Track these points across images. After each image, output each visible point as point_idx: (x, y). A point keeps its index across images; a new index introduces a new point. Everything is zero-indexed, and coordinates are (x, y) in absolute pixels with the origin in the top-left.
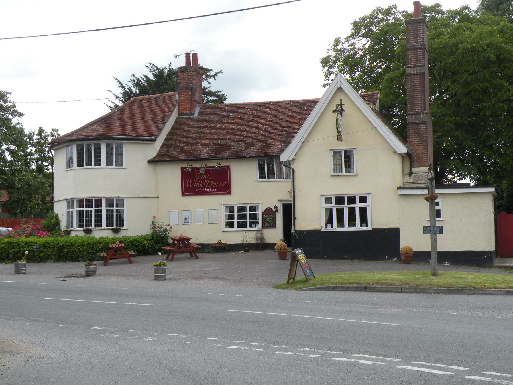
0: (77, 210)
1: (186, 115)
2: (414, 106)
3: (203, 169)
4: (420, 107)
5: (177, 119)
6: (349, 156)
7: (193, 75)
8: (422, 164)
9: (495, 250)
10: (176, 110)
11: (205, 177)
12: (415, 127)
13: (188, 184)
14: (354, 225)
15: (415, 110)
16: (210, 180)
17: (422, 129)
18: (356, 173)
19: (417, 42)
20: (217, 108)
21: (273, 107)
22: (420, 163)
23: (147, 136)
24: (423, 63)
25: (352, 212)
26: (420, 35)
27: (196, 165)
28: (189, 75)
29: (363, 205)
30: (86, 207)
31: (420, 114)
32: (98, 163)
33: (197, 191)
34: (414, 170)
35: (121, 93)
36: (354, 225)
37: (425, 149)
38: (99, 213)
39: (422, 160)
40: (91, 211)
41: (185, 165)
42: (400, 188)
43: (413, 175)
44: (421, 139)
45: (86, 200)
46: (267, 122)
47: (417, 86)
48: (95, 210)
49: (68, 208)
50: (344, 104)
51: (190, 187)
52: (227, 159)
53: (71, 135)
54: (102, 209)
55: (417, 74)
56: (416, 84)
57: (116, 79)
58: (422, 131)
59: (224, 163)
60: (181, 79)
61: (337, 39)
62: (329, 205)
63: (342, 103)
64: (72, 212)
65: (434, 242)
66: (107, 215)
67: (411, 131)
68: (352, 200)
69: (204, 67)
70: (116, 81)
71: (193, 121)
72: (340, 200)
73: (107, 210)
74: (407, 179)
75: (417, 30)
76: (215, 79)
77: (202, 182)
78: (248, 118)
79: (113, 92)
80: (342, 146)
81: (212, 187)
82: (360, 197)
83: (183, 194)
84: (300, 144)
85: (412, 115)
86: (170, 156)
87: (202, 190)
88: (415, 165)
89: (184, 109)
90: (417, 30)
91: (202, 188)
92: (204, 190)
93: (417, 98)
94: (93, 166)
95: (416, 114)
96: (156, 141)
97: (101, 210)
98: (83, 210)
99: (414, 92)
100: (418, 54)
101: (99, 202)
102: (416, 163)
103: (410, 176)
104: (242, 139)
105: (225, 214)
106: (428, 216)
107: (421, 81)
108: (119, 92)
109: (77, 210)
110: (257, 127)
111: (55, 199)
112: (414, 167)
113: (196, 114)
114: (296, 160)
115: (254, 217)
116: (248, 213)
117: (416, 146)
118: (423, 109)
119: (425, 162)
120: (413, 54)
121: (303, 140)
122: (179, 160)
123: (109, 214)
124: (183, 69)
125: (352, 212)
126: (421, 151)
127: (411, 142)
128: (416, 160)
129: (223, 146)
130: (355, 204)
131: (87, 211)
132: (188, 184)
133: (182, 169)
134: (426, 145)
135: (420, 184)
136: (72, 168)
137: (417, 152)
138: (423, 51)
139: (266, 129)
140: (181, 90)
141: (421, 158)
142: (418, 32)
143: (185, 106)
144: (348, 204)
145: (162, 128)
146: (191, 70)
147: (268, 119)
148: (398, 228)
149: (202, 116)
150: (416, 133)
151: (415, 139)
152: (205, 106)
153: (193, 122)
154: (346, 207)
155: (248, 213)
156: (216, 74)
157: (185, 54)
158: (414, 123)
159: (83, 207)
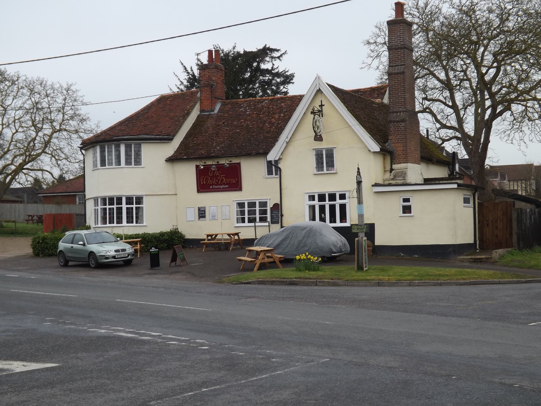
0: (101, 208)
1: (207, 112)
2: (395, 104)
3: (214, 166)
4: (401, 105)
5: (198, 116)
6: (330, 154)
7: (213, 72)
8: (402, 161)
9: (375, 245)
10: (197, 107)
11: (218, 174)
12: (395, 125)
13: (203, 181)
15: (396, 108)
16: (222, 177)
17: (402, 126)
18: (336, 171)
19: (398, 42)
20: (237, 104)
21: (289, 102)
22: (400, 160)
23: (166, 134)
24: (403, 63)
25: (332, 208)
26: (401, 35)
27: (209, 163)
28: (210, 73)
29: (342, 202)
30: (109, 205)
31: (400, 112)
32: (119, 163)
33: (211, 187)
34: (395, 166)
35: (186, 79)
36: (335, 222)
37: (405, 146)
38: (120, 210)
39: (402, 157)
40: (113, 208)
41: (201, 164)
42: (376, 185)
43: (393, 172)
44: (401, 136)
45: (109, 198)
46: (281, 118)
47: (397, 84)
48: (117, 207)
49: (95, 206)
50: (324, 105)
51: (205, 183)
53: (100, 135)
54: (126, 205)
55: (397, 73)
56: (397, 82)
57: (182, 64)
58: (401, 128)
59: (235, 161)
60: (202, 77)
62: (312, 203)
63: (323, 104)
64: (97, 209)
66: (128, 213)
68: (332, 197)
69: (270, 47)
70: (181, 66)
71: (212, 118)
72: (322, 197)
73: (127, 208)
74: (388, 175)
75: (398, 30)
76: (280, 60)
77: (216, 179)
78: (264, 113)
79: (179, 77)
81: (224, 184)
82: (248, 202)
83: (199, 191)
84: (285, 145)
85: (393, 112)
86: (185, 155)
87: (216, 187)
88: (396, 161)
89: (205, 106)
90: (398, 30)
91: (216, 185)
92: (217, 187)
93: (398, 96)
95: (397, 112)
97: (122, 207)
98: (106, 208)
99: (395, 91)
100: (398, 53)
101: (119, 200)
102: (396, 160)
103: (391, 172)
104: (254, 135)
105: (237, 210)
106: (400, 211)
107: (401, 80)
108: (184, 77)
109: (101, 208)
110: (270, 123)
111: (87, 197)
112: (395, 164)
113: (216, 111)
114: (282, 160)
115: (264, 212)
116: (257, 208)
117: (397, 143)
118: (404, 107)
119: (404, 158)
120: (395, 54)
121: (287, 140)
122: (193, 158)
123: (129, 211)
124: (204, 67)
125: (332, 208)
126: (401, 148)
127: (392, 139)
128: (396, 157)
129: (235, 143)
130: (336, 201)
131: (109, 208)
132: (203, 181)
133: (197, 167)
134: (405, 142)
135: (399, 181)
136: (96, 168)
137: (398, 149)
138: (403, 51)
139: (278, 124)
140: (203, 87)
141: (401, 155)
142: (399, 32)
143: (206, 103)
144: (329, 201)
145: (180, 126)
146: (212, 67)
147: (282, 115)
148: (374, 224)
149: (221, 113)
150: (397, 131)
151: (396, 137)
152: (225, 102)
153: (212, 119)
154: (327, 203)
155: (257, 208)
156: (281, 56)
157: (208, 52)
159: (106, 205)
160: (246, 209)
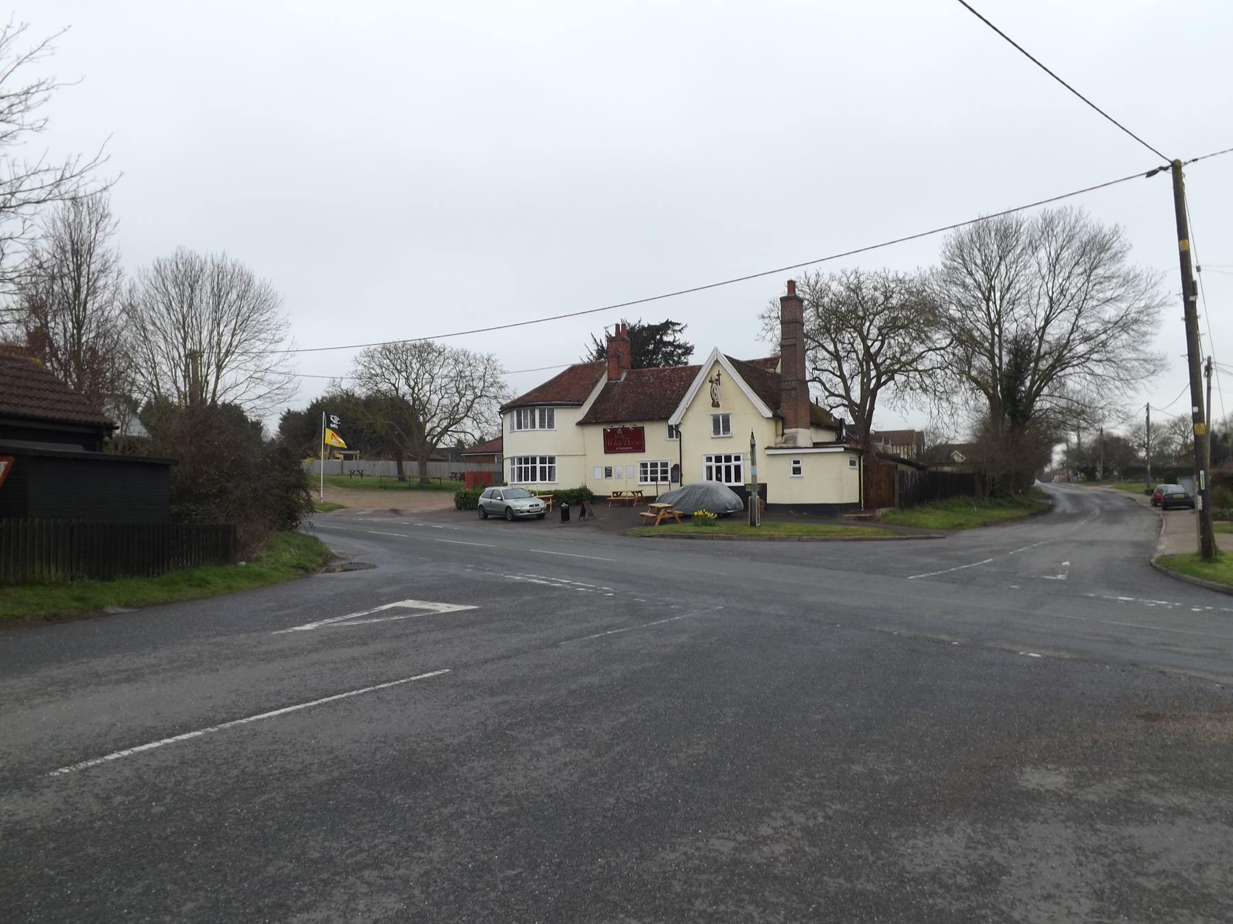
6: (726, 420)
14: (730, 481)
25: (728, 469)
34: (785, 431)
36: (730, 481)
38: (534, 469)
41: (608, 428)
42: (768, 448)
52: (640, 421)
59: (639, 425)
61: (981, 228)
62: (709, 464)
65: (1148, 486)
67: (784, 397)
68: (728, 459)
72: (718, 459)
74: (779, 439)
80: (720, 411)
81: (629, 446)
83: (605, 452)
94: (529, 429)
96: (582, 405)
108: (594, 348)
113: (622, 379)
116: (659, 468)
123: (543, 469)
125: (728, 469)
133: (605, 430)
155: (659, 468)
158: (786, 390)
160: (649, 469)
